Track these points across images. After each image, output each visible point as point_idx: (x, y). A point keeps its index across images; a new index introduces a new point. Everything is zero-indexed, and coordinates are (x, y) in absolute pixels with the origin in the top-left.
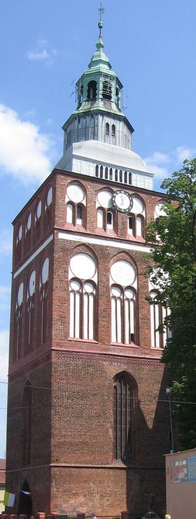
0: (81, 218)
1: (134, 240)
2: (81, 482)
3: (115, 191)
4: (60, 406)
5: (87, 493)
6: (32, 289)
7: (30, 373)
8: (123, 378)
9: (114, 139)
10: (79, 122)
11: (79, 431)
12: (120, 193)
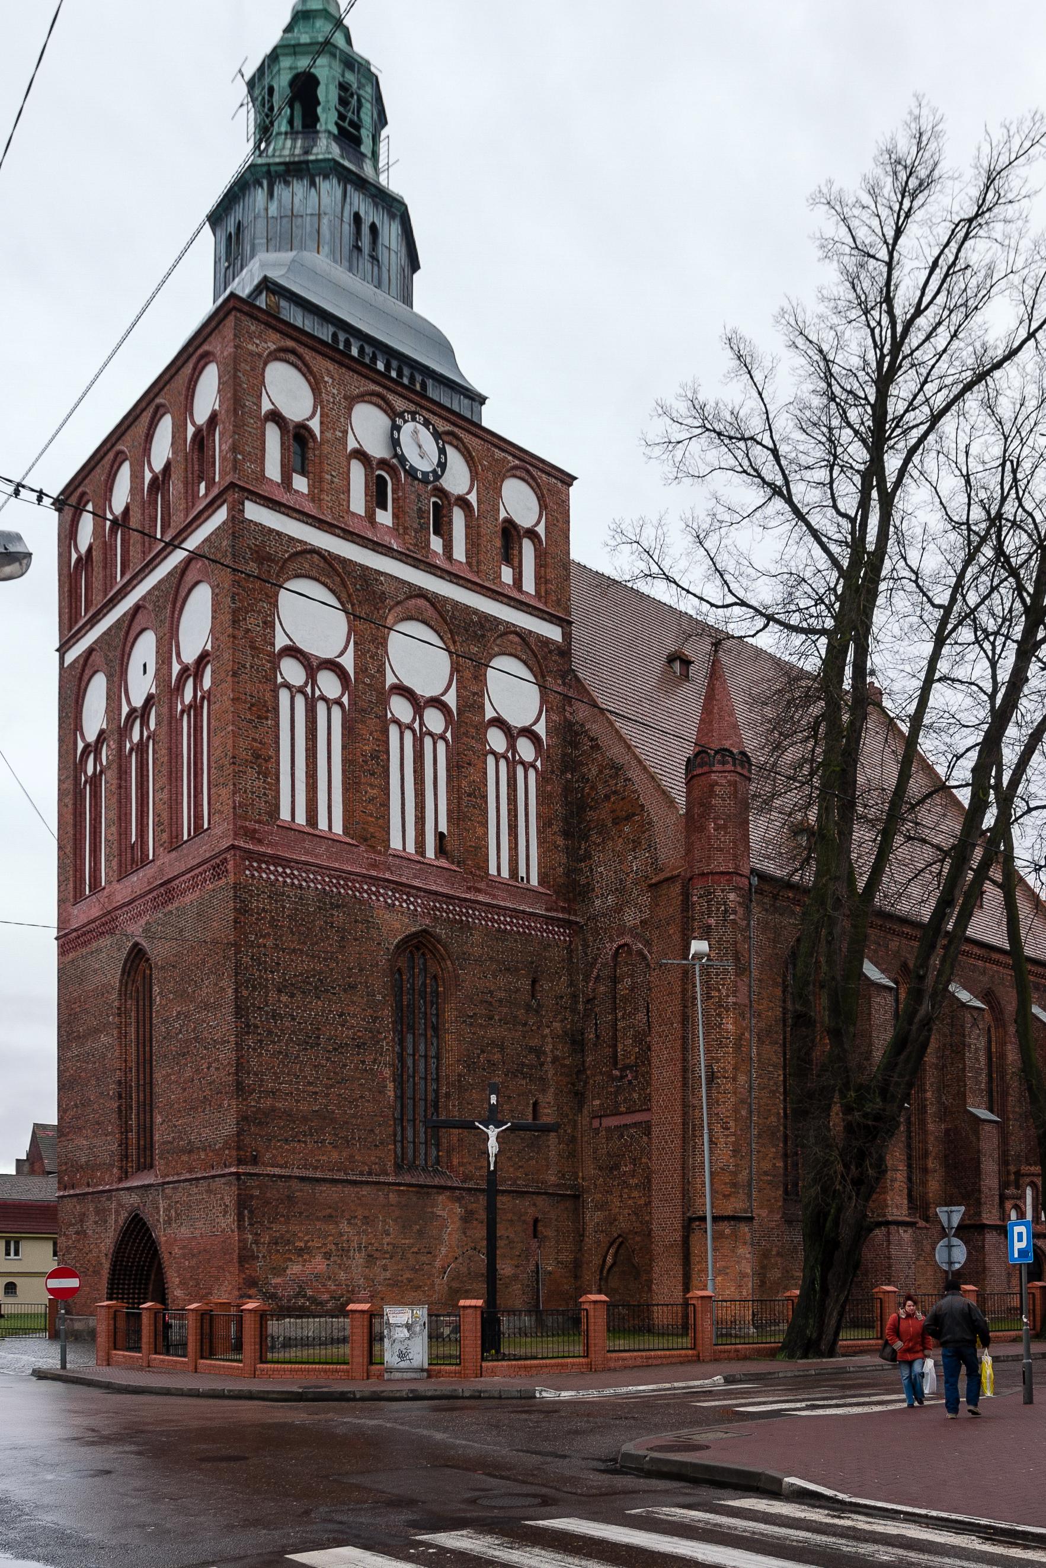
0: (303, 473)
1: (446, 566)
2: (318, 1219)
3: (399, 409)
4: (259, 1008)
5: (333, 1247)
6: (140, 685)
7: (143, 922)
8: (418, 944)
9: (376, 269)
10: (271, 194)
11: (310, 1084)
12: (414, 419)
